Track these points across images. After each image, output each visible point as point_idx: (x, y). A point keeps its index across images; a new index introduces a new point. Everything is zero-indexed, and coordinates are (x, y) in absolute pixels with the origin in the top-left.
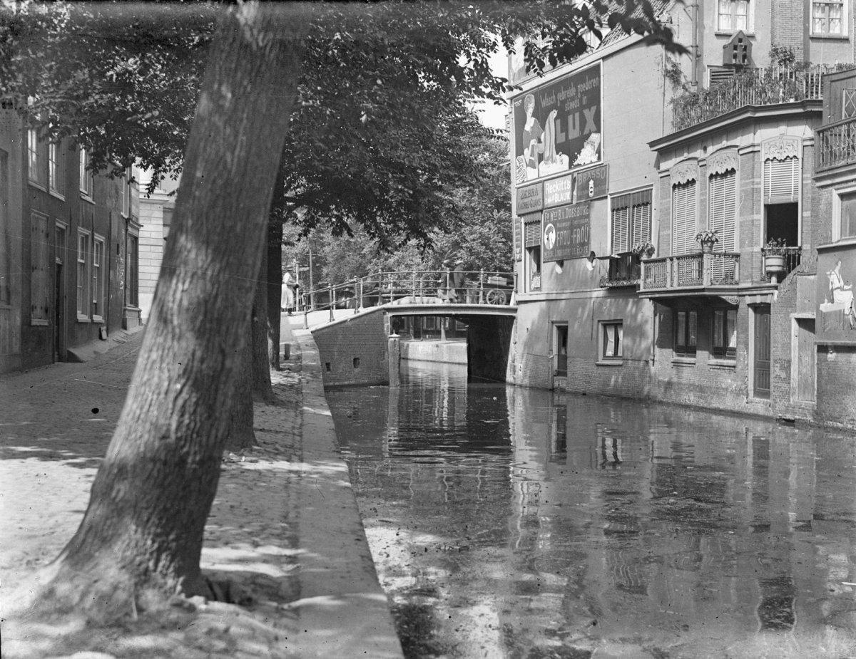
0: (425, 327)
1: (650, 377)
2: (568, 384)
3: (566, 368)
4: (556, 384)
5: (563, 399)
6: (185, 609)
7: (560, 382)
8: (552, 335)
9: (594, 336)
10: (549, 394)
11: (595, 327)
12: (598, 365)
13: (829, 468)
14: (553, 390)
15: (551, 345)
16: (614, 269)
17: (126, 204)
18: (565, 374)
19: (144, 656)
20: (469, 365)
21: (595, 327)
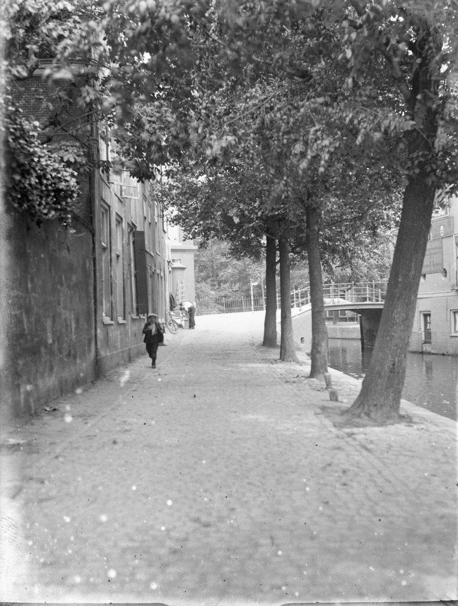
0: (328, 315)
1: (427, 69)
2: (432, 348)
3: (430, 339)
4: (424, 349)
5: (428, 358)
6: (49, 565)
7: (427, 348)
8: (420, 320)
9: (448, 319)
10: (420, 355)
11: (449, 314)
12: (452, 336)
13: (252, 53)
14: (422, 353)
15: (420, 326)
16: (357, 405)
17: (107, 228)
18: (430, 343)
19: (14, 605)
20: (362, 339)
21: (449, 314)
